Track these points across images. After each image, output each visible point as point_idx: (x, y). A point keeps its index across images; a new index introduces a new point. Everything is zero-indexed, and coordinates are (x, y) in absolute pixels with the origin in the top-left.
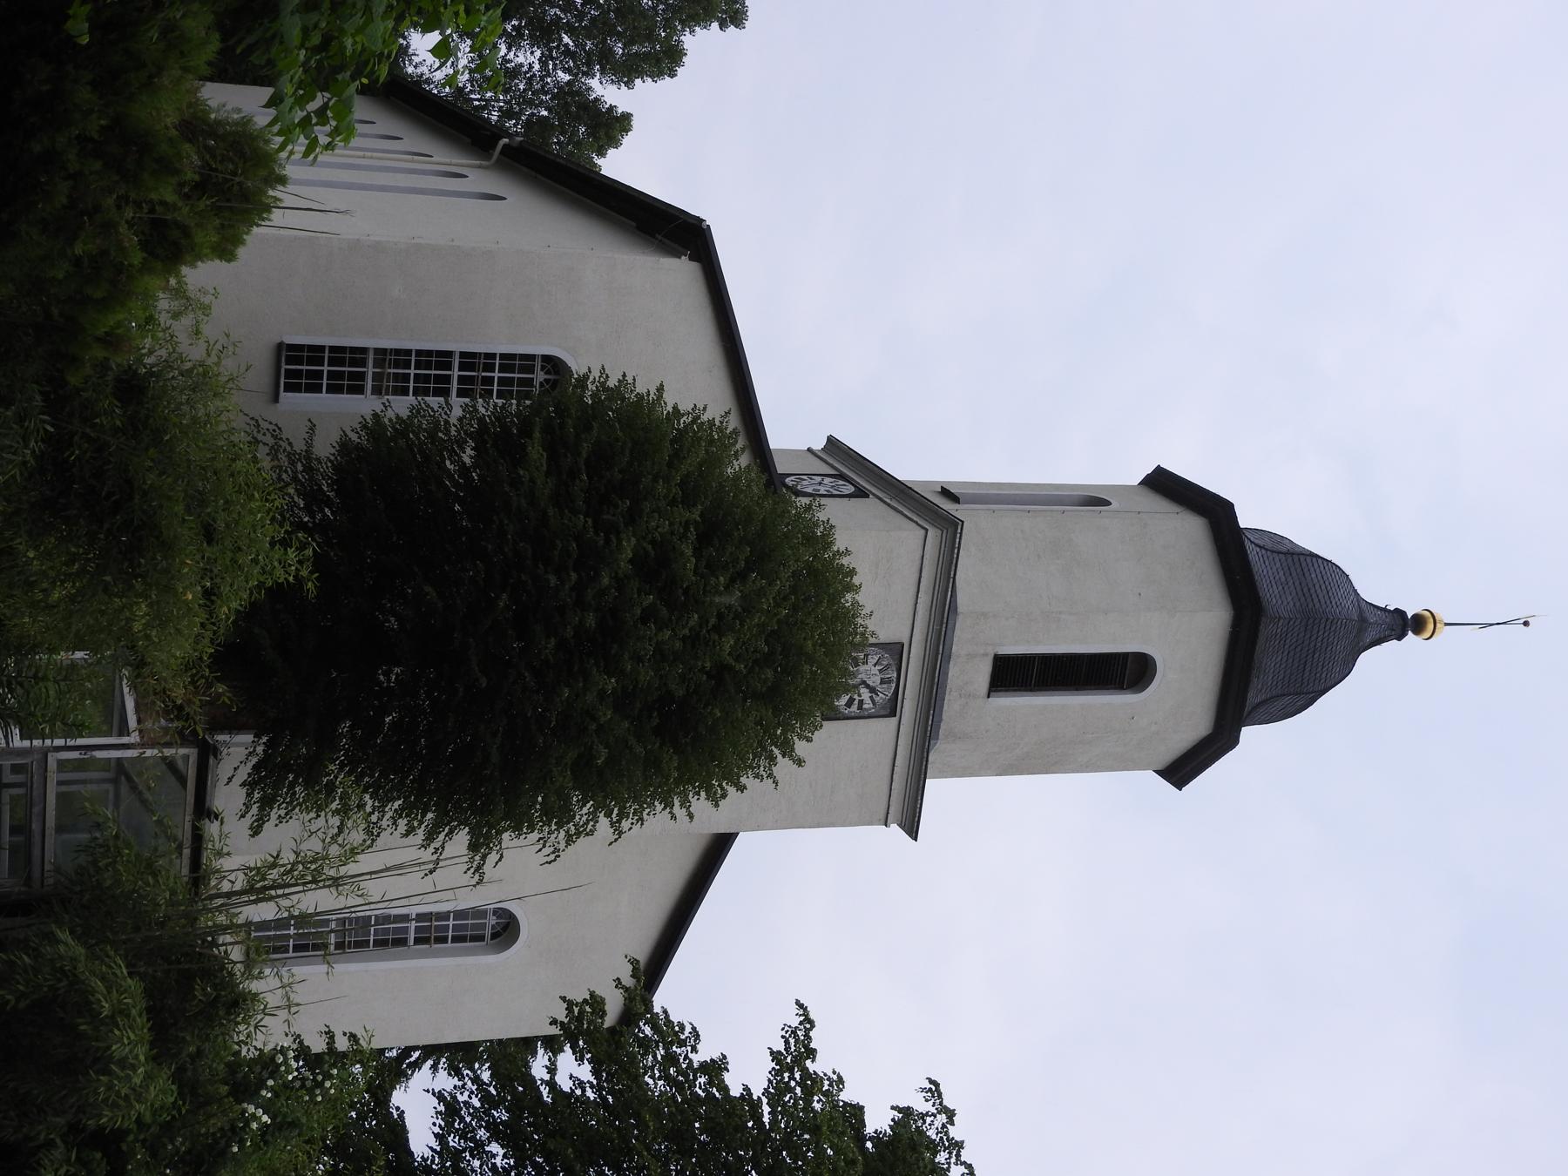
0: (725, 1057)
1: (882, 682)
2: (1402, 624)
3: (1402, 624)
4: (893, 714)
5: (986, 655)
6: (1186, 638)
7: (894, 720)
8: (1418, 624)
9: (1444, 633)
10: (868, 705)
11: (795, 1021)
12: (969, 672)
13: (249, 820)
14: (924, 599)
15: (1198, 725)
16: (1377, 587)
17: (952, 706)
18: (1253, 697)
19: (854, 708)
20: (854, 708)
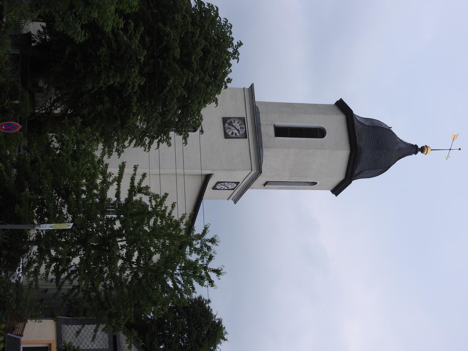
0: (138, 165)
1: (241, 128)
2: (413, 149)
3: (413, 149)
4: (246, 137)
5: (271, 125)
6: (333, 153)
7: (247, 139)
8: (422, 150)
9: (430, 153)
10: (238, 134)
11: (161, 143)
12: (268, 131)
13: (140, 172)
14: (248, 107)
15: (340, 177)
16: (405, 134)
17: (265, 139)
18: (357, 172)
19: (234, 135)
20: (234, 135)
